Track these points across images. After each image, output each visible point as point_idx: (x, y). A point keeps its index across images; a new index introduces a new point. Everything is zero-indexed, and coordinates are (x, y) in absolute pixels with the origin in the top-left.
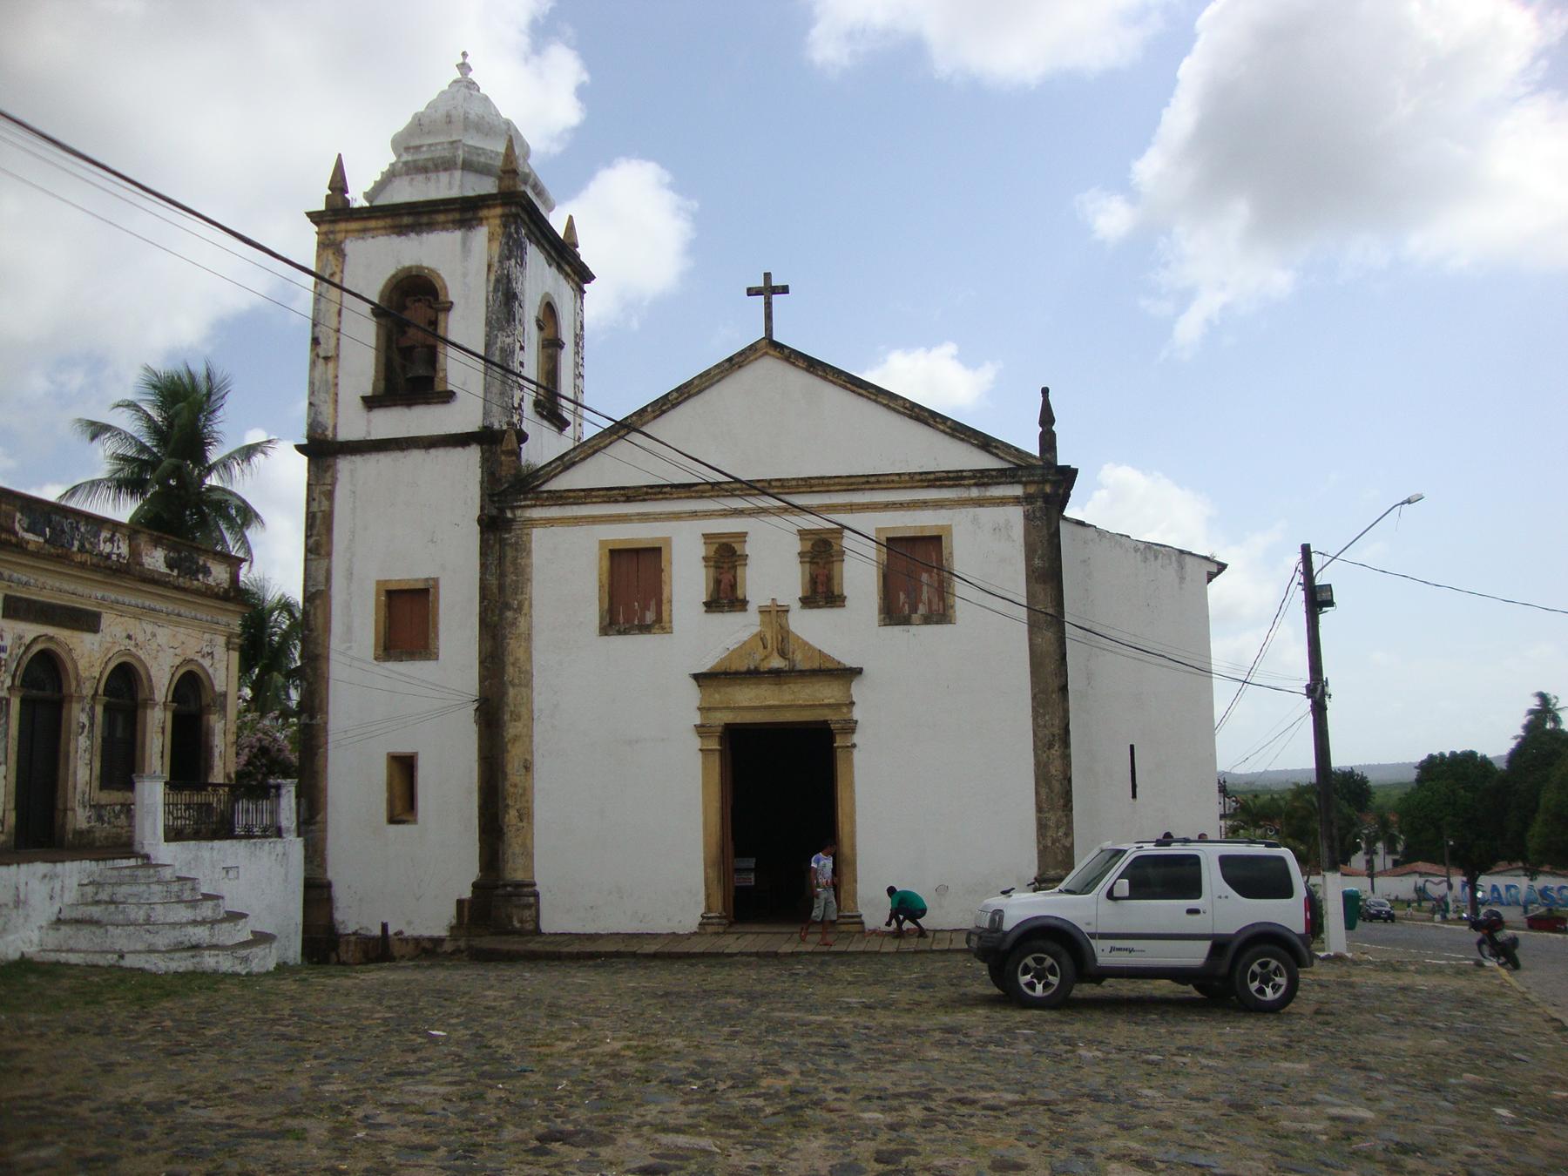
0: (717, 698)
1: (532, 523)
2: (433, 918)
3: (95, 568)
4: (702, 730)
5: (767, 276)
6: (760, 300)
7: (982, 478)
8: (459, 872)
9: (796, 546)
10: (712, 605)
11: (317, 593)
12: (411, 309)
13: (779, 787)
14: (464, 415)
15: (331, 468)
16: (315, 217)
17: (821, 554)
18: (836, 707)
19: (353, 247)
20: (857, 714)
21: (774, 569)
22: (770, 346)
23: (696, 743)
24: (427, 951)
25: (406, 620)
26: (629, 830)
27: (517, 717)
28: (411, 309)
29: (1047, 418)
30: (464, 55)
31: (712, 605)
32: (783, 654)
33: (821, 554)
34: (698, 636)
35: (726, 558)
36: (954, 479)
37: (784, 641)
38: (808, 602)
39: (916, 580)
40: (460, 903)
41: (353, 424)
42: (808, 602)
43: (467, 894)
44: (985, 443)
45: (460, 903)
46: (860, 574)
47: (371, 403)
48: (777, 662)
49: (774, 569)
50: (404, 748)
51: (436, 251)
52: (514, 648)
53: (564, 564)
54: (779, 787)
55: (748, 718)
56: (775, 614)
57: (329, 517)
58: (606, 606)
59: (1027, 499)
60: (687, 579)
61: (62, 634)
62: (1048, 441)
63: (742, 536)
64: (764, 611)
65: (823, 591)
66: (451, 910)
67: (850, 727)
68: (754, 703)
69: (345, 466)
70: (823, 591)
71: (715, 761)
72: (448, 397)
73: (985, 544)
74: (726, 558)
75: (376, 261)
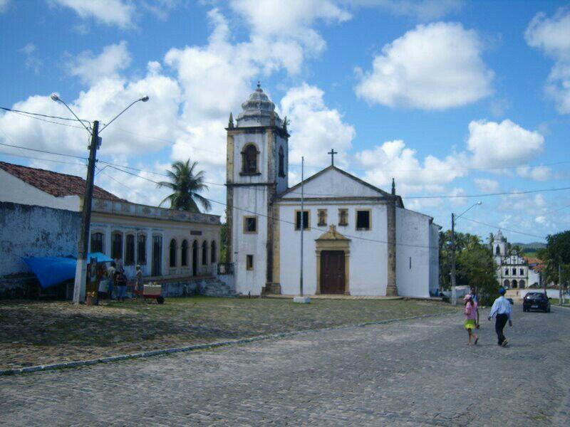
0: (320, 245)
1: (279, 205)
2: (258, 292)
3: (169, 220)
4: (317, 252)
5: (336, 153)
6: (331, 155)
7: (378, 199)
8: (262, 281)
9: (338, 212)
10: (319, 225)
11: (229, 219)
12: (250, 154)
13: (333, 267)
14: (265, 178)
15: (232, 189)
16: (226, 129)
17: (343, 214)
18: (346, 247)
19: (235, 137)
20: (350, 249)
21: (333, 217)
22: (332, 167)
23: (316, 255)
24: (257, 297)
25: (251, 225)
26: (298, 267)
27: (276, 247)
28: (250, 154)
29: (393, 185)
30: (259, 86)
31: (319, 225)
32: (334, 236)
33: (343, 214)
34: (315, 232)
35: (322, 214)
36: (371, 198)
37: (335, 233)
38: (340, 225)
39: (364, 221)
40: (263, 288)
41: (237, 179)
42: (340, 225)
43: (265, 286)
44: (379, 191)
45: (263, 288)
46: (352, 219)
47: (241, 175)
48: (333, 237)
49: (333, 217)
50: (250, 253)
51: (257, 139)
52: (275, 257)
53: (287, 214)
54: (333, 267)
55: (325, 249)
56: (333, 227)
57: (232, 200)
58: (285, 158)
59: (386, 204)
60: (314, 219)
61: (197, 236)
62: (393, 190)
63: (326, 210)
64: (330, 226)
65: (343, 223)
66: (261, 289)
67: (349, 252)
68: (328, 246)
69: (235, 190)
70: (343, 223)
71: (319, 258)
72: (259, 174)
73: (379, 216)
74: (322, 214)
75: (242, 141)
